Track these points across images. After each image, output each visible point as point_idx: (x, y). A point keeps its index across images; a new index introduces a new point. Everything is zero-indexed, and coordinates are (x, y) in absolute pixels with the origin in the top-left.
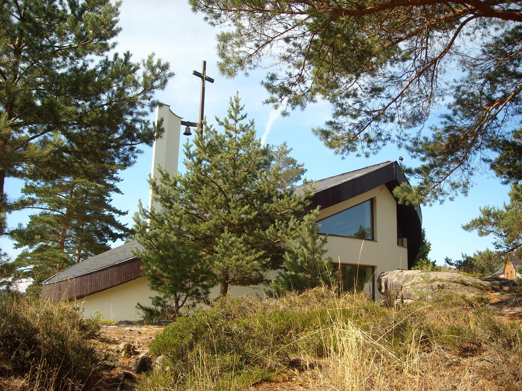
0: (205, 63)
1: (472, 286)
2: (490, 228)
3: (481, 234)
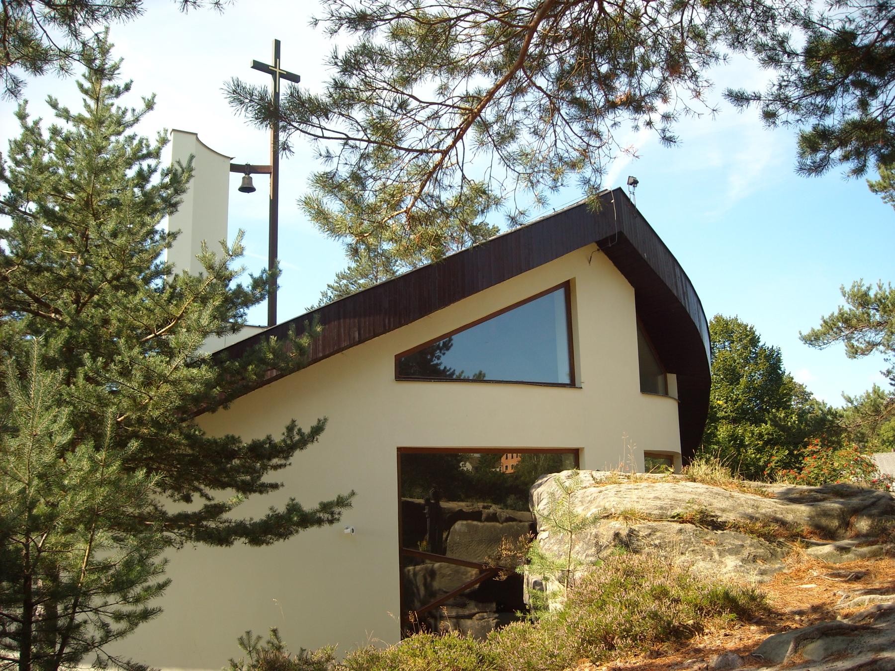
0: (277, 44)
1: (736, 527)
2: (871, 336)
3: (854, 352)
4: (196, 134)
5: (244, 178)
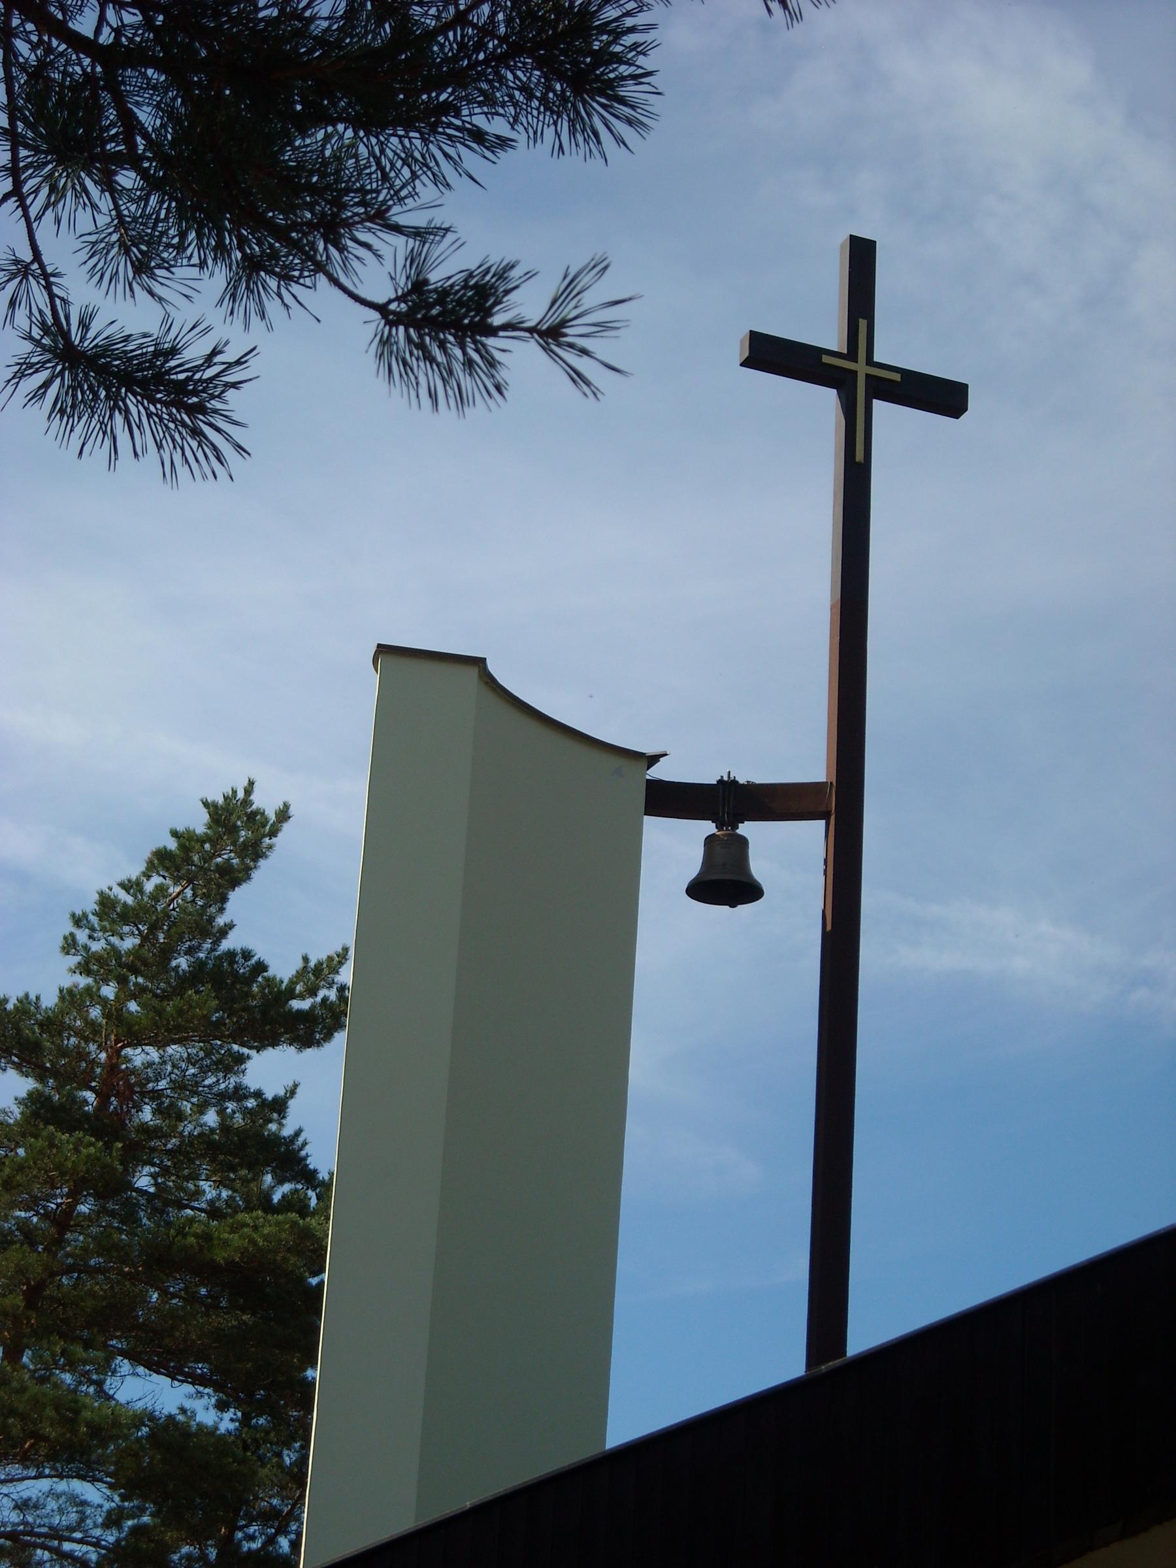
0: (862, 254)
4: (480, 662)
5: (710, 841)
